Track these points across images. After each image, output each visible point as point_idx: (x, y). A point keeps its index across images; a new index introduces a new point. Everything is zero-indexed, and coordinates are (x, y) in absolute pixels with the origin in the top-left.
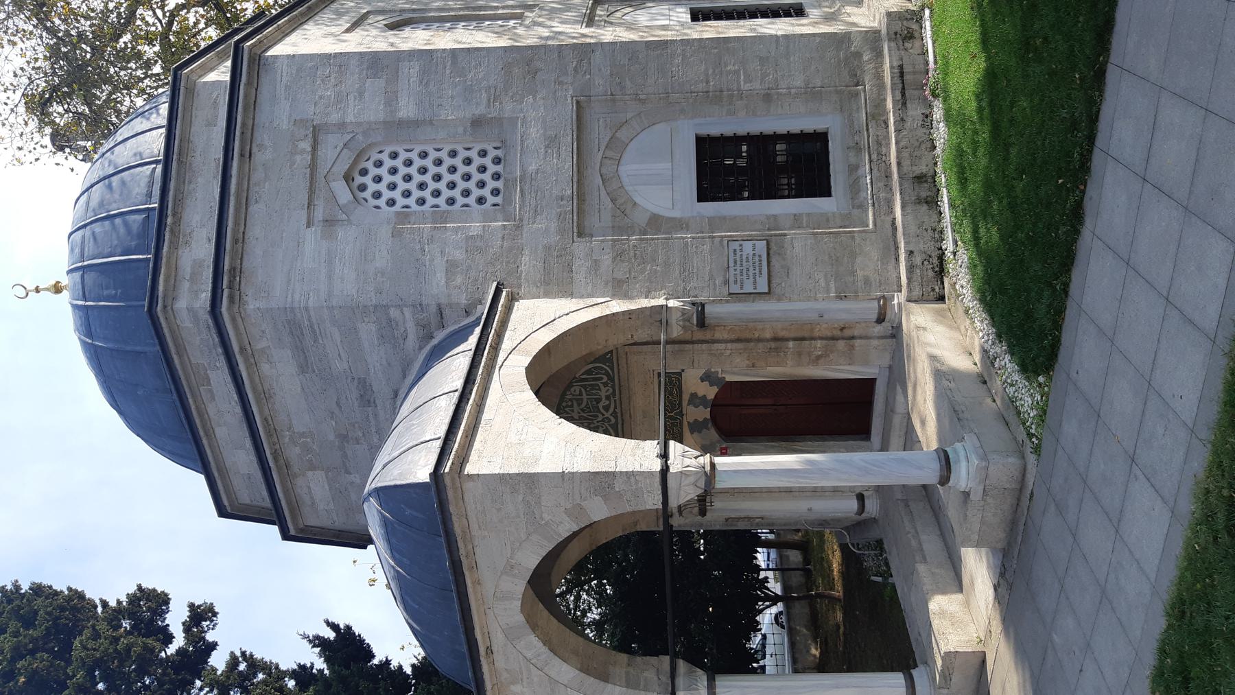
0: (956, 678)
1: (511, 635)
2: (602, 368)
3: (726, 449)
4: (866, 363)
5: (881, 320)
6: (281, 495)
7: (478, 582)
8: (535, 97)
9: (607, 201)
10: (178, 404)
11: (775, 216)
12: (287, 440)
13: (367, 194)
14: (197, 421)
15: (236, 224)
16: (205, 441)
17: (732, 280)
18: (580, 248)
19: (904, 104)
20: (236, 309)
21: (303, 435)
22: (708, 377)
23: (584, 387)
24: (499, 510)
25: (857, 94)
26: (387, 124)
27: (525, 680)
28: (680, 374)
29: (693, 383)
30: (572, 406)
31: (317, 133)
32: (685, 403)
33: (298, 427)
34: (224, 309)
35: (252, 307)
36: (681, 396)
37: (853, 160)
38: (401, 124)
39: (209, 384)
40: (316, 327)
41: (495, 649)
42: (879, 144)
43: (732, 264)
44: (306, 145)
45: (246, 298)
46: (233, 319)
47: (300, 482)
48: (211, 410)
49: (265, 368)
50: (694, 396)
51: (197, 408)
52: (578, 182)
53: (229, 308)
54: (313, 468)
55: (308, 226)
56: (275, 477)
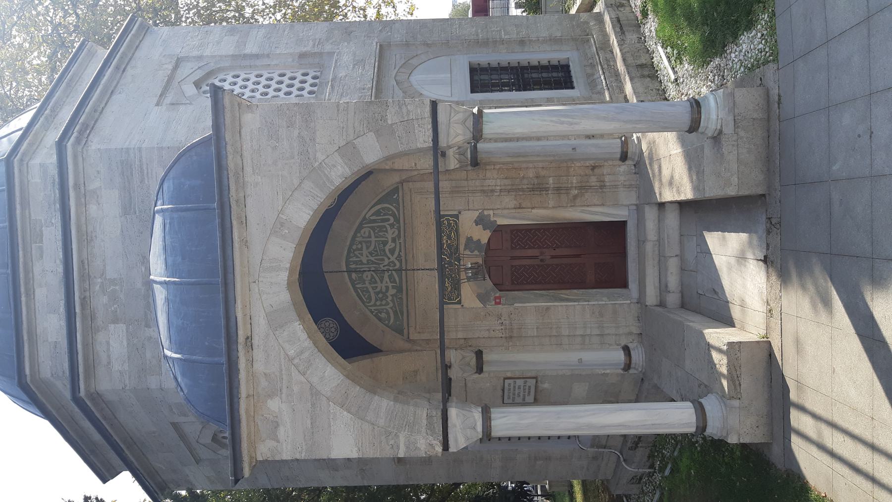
0: (746, 382)
1: (275, 323)
2: (389, 209)
3: (499, 298)
4: (616, 205)
5: (624, 157)
6: (79, 346)
7: (245, 243)
8: (348, 43)
10: (10, 278)
12: (97, 288)
14: (22, 276)
15: (99, 100)
16: (23, 299)
20: (80, 149)
21: (113, 281)
22: (481, 221)
23: (373, 228)
24: (275, 148)
25: (588, 41)
26: (234, 57)
27: (284, 390)
28: (457, 216)
29: (471, 229)
30: (361, 249)
31: (179, 62)
32: (462, 247)
33: (111, 274)
34: (69, 145)
35: (93, 148)
36: (458, 239)
37: (589, 70)
38: (245, 56)
39: (41, 241)
40: (145, 167)
41: (256, 341)
42: (607, 61)
45: (90, 143)
46: (75, 157)
47: (101, 337)
48: (37, 269)
49: (93, 209)
50: (469, 239)
51: (25, 264)
52: (377, 82)
53: (73, 145)
54: (115, 321)
56: (78, 324)
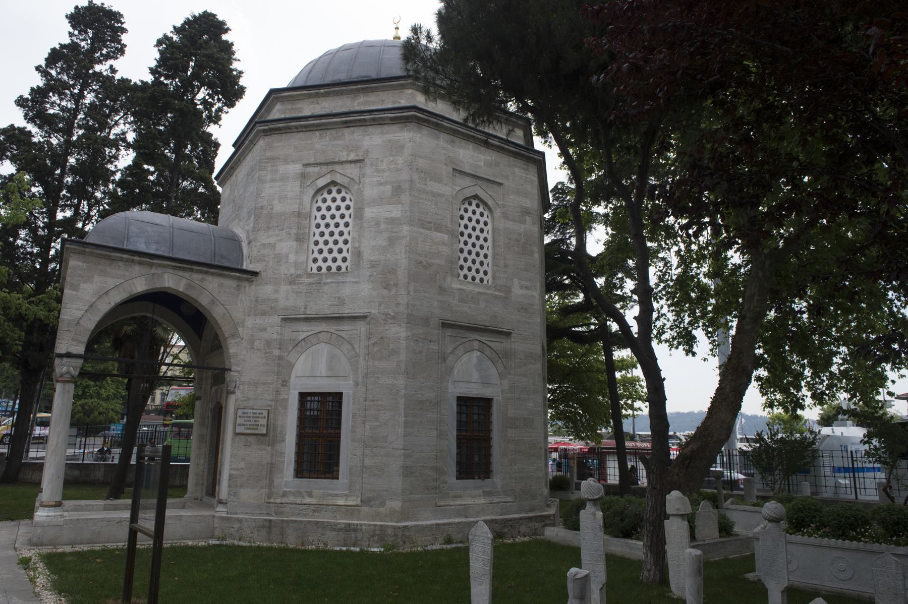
9: (302, 336)
11: (283, 441)
13: (466, 205)
17: (245, 411)
18: (276, 319)
19: (335, 530)
43: (254, 411)
44: (352, 157)
55: (454, 169)
